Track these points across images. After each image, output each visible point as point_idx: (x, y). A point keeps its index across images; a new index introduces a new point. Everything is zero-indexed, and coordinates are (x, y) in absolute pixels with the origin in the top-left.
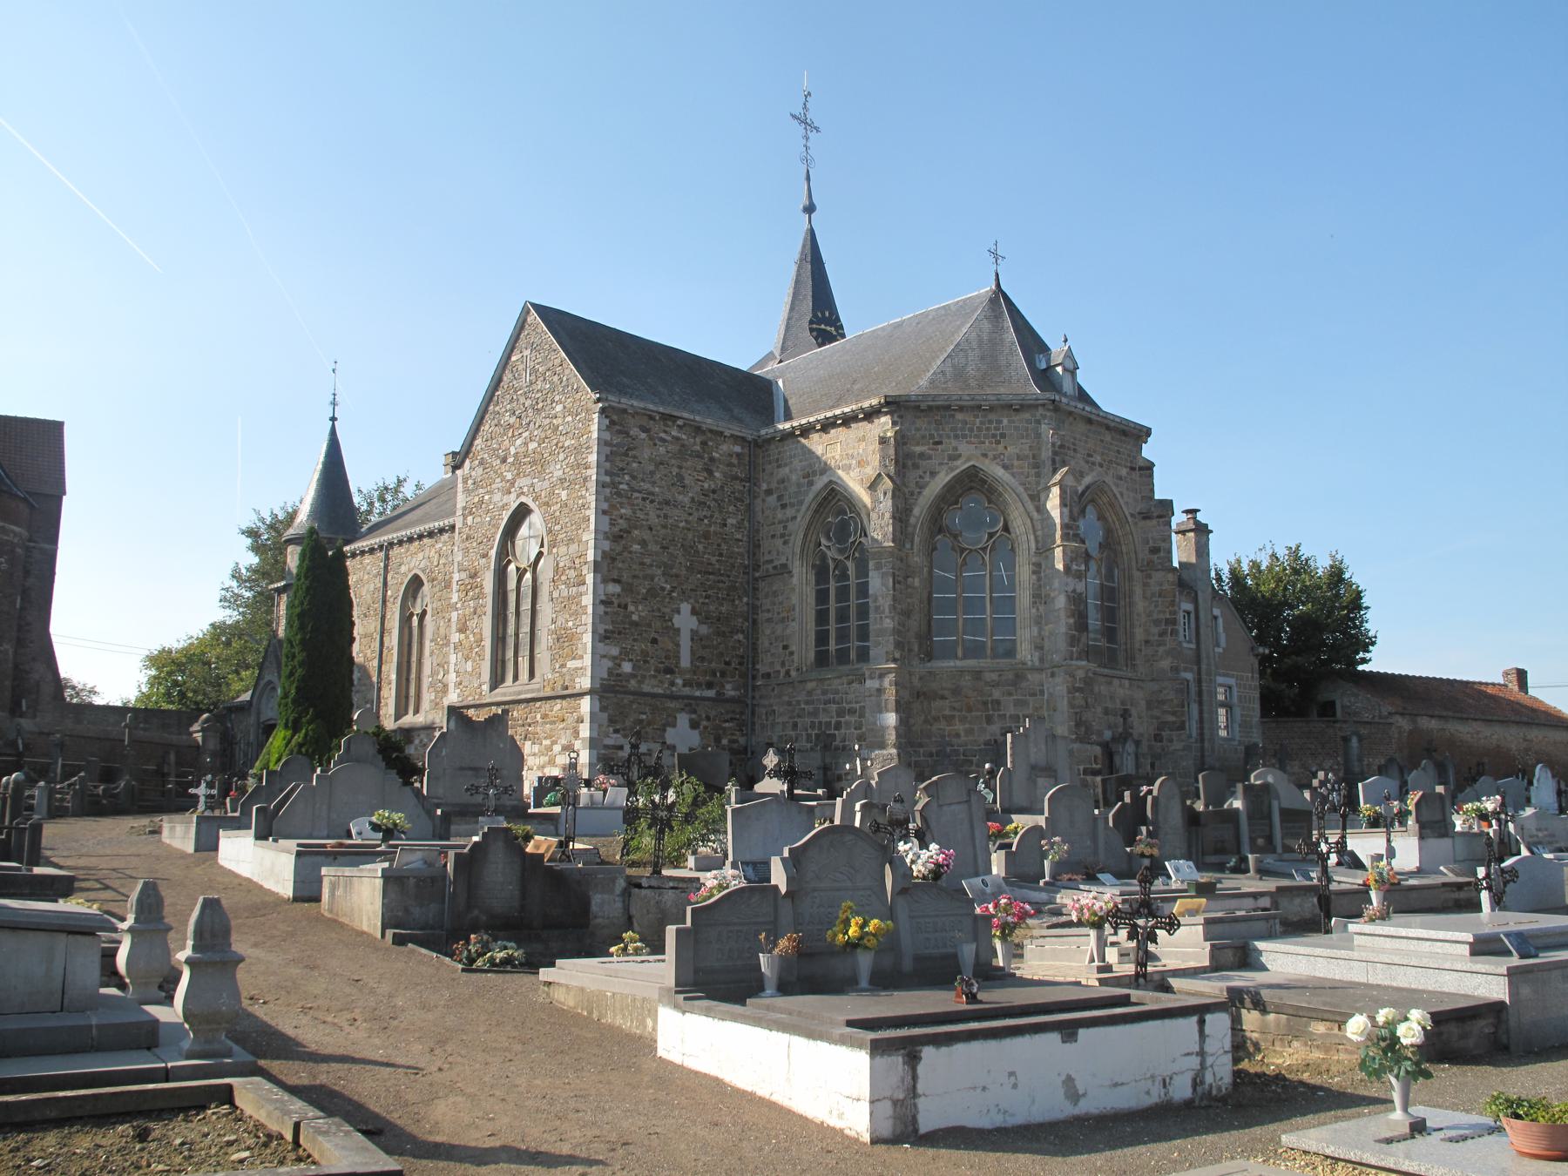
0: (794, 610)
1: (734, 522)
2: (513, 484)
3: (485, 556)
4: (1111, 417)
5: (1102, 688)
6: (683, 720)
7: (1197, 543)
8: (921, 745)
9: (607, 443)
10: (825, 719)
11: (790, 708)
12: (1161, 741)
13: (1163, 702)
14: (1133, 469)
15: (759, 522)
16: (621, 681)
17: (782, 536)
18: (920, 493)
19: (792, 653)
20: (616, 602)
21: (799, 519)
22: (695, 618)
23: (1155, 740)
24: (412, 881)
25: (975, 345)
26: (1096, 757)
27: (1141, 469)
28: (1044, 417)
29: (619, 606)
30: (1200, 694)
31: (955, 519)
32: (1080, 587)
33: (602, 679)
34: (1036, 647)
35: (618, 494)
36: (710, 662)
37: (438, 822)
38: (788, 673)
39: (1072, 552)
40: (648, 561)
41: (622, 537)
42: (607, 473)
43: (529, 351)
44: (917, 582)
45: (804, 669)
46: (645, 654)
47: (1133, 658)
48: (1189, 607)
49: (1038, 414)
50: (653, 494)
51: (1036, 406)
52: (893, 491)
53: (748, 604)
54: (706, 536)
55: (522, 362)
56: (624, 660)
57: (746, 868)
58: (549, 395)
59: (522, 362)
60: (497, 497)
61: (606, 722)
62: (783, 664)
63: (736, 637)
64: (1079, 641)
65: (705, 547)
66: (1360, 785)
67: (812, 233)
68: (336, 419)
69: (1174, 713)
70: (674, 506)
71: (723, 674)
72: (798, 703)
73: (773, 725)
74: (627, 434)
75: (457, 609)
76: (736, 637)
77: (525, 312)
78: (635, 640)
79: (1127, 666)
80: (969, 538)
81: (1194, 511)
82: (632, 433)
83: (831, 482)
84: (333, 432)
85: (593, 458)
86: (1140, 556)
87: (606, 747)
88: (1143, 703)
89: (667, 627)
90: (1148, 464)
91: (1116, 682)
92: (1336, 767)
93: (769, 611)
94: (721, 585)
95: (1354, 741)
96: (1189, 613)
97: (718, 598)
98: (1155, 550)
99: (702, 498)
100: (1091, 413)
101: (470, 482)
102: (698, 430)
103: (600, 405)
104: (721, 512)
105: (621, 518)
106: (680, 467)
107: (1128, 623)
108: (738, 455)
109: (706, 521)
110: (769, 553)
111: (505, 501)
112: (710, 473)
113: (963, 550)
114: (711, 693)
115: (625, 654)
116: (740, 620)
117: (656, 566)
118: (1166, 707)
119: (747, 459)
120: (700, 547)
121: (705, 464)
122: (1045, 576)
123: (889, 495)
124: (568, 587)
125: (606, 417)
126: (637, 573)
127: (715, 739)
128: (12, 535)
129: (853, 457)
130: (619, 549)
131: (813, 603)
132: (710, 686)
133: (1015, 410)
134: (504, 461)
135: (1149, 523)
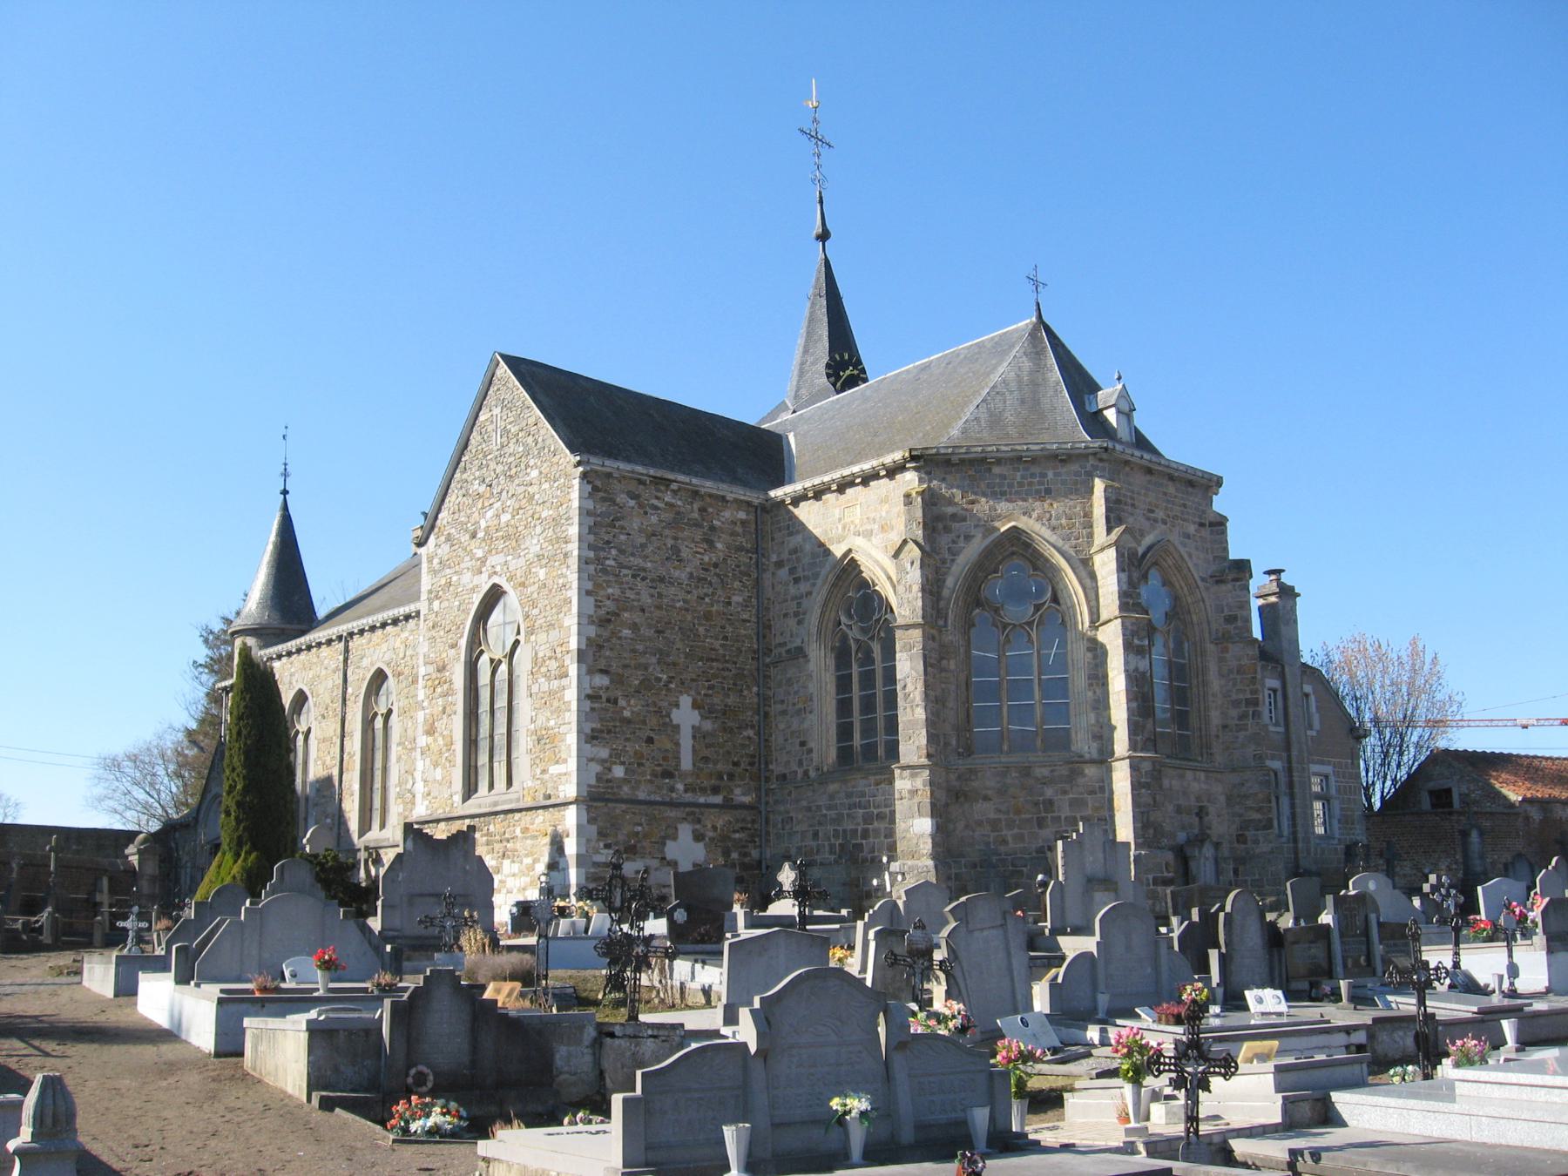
0: (811, 700)
1: (740, 599)
2: (483, 561)
3: (454, 646)
4: (1175, 466)
6: (685, 831)
11: (809, 814)
13: (1246, 797)
14: (1202, 525)
16: (612, 788)
17: (796, 614)
18: (953, 560)
19: (810, 751)
21: (814, 594)
22: (696, 712)
23: (1238, 842)
25: (1013, 386)
26: (1167, 864)
27: (1211, 524)
29: (608, 701)
30: (1291, 785)
31: (996, 589)
33: (589, 786)
35: (605, 571)
36: (715, 763)
39: (1133, 624)
40: (640, 648)
43: (499, 409)
48: (1274, 683)
50: (644, 570)
51: (1085, 456)
56: (615, 763)
58: (523, 459)
60: (467, 577)
62: (800, 763)
64: (1144, 727)
68: (288, 492)
69: (1259, 810)
70: (669, 582)
71: (731, 776)
72: (819, 807)
75: (423, 708)
76: (745, 734)
78: (627, 740)
79: (1202, 756)
80: (1016, 613)
81: (1278, 572)
83: (850, 551)
84: (285, 507)
85: (574, 531)
86: (1214, 626)
87: (596, 864)
88: (1222, 799)
89: (665, 724)
90: (1219, 519)
94: (726, 673)
96: (1275, 691)
98: (1231, 619)
99: (703, 574)
101: (436, 561)
103: (581, 469)
106: (676, 539)
108: (743, 522)
109: (707, 600)
111: (475, 583)
112: (711, 543)
113: (1005, 626)
114: (718, 799)
115: (616, 756)
118: (1249, 803)
119: (754, 526)
120: (701, 630)
121: (705, 534)
123: (917, 564)
125: (588, 482)
130: (606, 634)
132: (715, 790)
133: (1062, 461)
134: (474, 536)
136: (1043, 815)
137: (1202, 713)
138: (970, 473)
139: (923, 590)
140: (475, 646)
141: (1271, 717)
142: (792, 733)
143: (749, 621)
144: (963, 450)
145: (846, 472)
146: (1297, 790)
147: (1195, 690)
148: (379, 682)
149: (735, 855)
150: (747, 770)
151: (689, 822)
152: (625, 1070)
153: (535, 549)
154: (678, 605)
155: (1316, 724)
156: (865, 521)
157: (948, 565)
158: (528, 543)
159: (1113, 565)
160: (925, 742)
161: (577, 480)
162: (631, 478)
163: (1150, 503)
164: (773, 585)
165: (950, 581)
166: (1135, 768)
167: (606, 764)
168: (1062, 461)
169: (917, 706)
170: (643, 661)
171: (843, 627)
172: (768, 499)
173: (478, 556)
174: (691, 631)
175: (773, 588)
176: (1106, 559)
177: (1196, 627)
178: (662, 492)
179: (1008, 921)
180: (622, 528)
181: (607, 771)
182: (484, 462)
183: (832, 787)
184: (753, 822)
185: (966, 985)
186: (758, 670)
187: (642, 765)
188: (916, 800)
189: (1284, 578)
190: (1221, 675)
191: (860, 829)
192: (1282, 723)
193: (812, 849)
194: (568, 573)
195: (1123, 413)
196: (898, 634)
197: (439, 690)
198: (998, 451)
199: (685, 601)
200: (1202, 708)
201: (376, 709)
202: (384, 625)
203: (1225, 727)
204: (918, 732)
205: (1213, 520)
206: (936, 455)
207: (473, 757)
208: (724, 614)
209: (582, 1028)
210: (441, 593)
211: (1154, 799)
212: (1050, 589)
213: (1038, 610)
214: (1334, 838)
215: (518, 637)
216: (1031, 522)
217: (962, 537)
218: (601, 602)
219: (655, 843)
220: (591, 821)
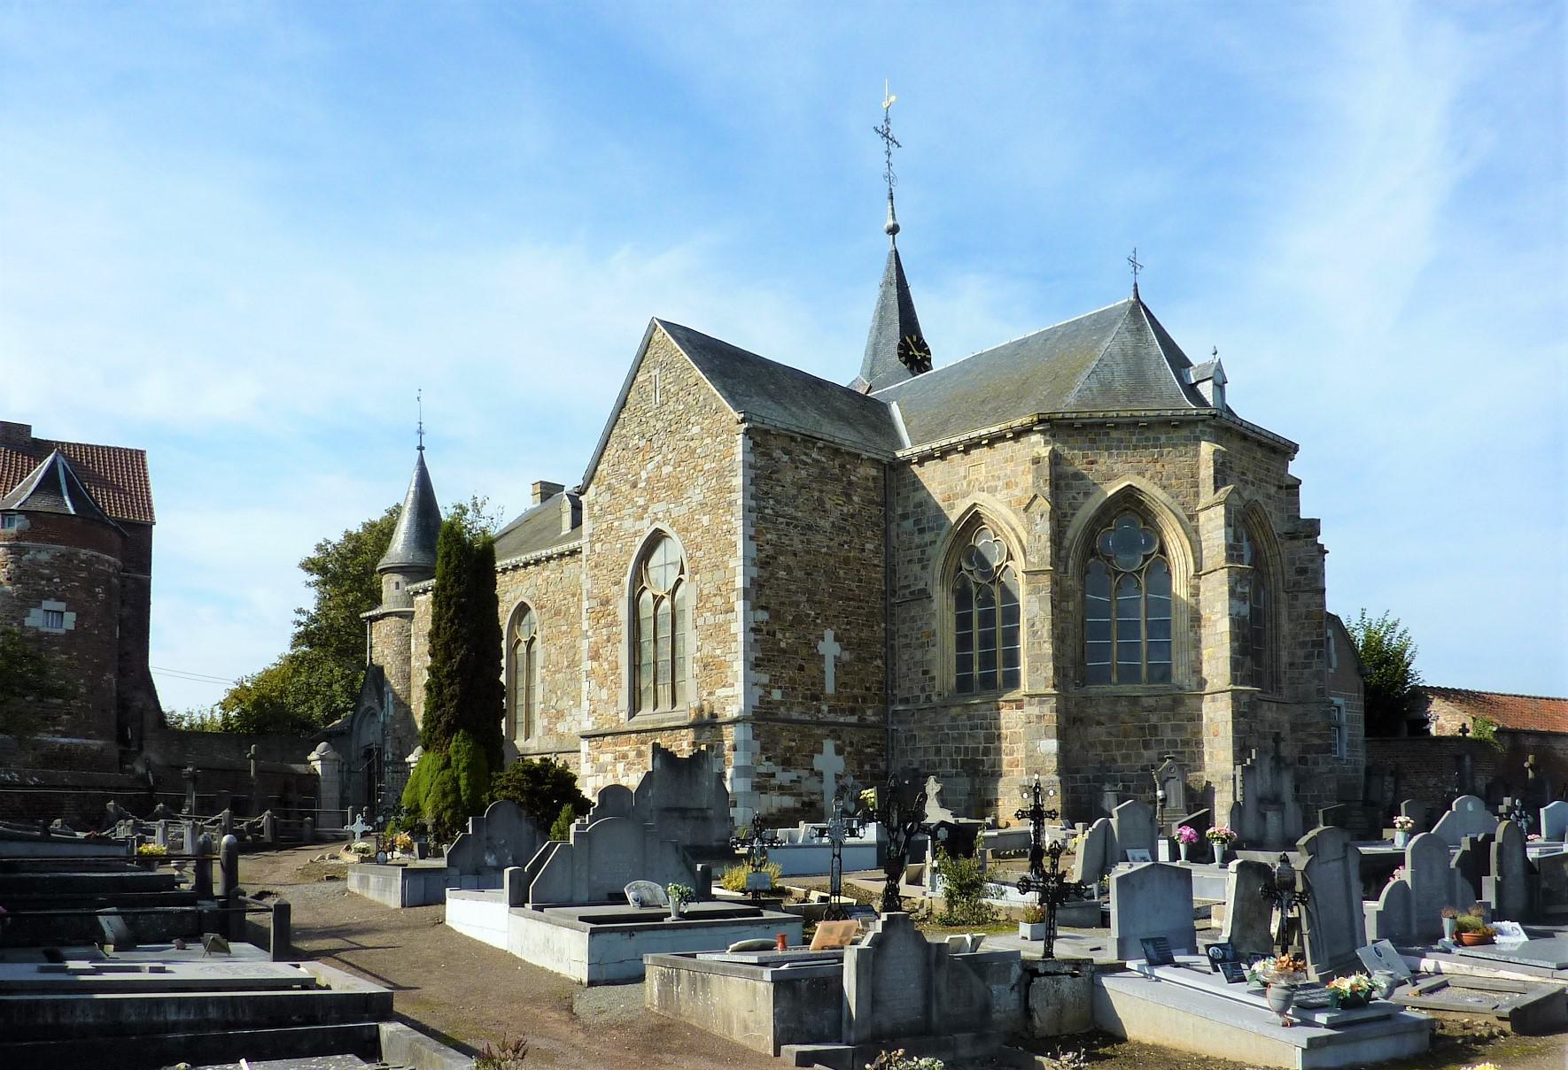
0: (934, 635)
2: (645, 508)
3: (617, 583)
4: (1258, 430)
6: (829, 746)
8: (1077, 771)
10: (970, 744)
11: (932, 733)
13: (1309, 725)
14: (1280, 487)
15: (894, 548)
17: (921, 560)
18: (1073, 514)
19: (933, 678)
20: (765, 629)
21: (939, 543)
22: (837, 644)
24: (804, 984)
25: (1119, 359)
27: (1288, 487)
33: (753, 707)
34: (1194, 672)
35: (764, 518)
36: (852, 688)
37: (699, 878)
38: (928, 698)
39: (1237, 573)
40: (793, 587)
43: (658, 371)
47: (1278, 681)
49: (1198, 431)
50: (795, 518)
54: (846, 561)
55: (651, 383)
57: (1147, 947)
58: (684, 416)
59: (651, 383)
60: (628, 523)
61: (758, 750)
62: (923, 689)
63: (875, 663)
64: (1243, 665)
68: (423, 448)
69: (1320, 736)
71: (864, 700)
72: (941, 728)
73: (913, 750)
75: (588, 637)
76: (875, 663)
77: (652, 328)
78: (783, 667)
79: (1272, 690)
80: (1122, 561)
82: (774, 455)
83: (975, 504)
84: (422, 463)
85: (738, 481)
87: (760, 775)
88: (1287, 726)
89: (813, 654)
92: (1440, 785)
93: (906, 636)
95: (1468, 759)
99: (843, 524)
101: (596, 508)
102: (836, 452)
103: (745, 426)
104: (859, 536)
107: (1274, 645)
108: (874, 478)
109: (846, 546)
110: (906, 577)
111: (637, 528)
112: (849, 496)
113: (1117, 573)
114: (853, 719)
116: (879, 646)
119: (883, 482)
120: (841, 572)
122: (1205, 599)
123: (1047, 516)
124: (714, 615)
125: (750, 438)
126: (783, 599)
127: (858, 764)
128: (107, 565)
129: (999, 478)
130: (766, 575)
131: (954, 628)
132: (852, 711)
134: (634, 486)
137: (1274, 652)
138: (1090, 436)
140: (637, 584)
143: (878, 566)
144: (1087, 415)
145: (974, 434)
148: (522, 613)
149: (867, 767)
151: (833, 739)
152: (1050, 1007)
154: (824, 550)
155: (1334, 664)
156: (990, 478)
158: (690, 493)
159: (1222, 521)
160: (1052, 674)
161: (741, 436)
162: (787, 436)
164: (898, 535)
165: (1070, 534)
167: (767, 689)
169: (1045, 642)
170: (794, 599)
171: (964, 572)
172: (895, 458)
173: (639, 504)
174: (834, 573)
175: (898, 538)
176: (1213, 515)
177: (1272, 577)
179: (1349, 854)
180: (779, 481)
181: (767, 694)
182: (644, 419)
183: (954, 711)
185: (1318, 916)
186: (886, 608)
188: (1043, 724)
190: (1291, 620)
191: (981, 747)
193: (935, 764)
194: (733, 519)
197: (603, 621)
200: (1274, 648)
201: (519, 637)
202: (526, 565)
203: (1291, 665)
204: (1045, 665)
205: (1290, 483)
207: (637, 678)
208: (860, 559)
209: (1008, 967)
210: (602, 536)
212: (1158, 541)
214: (1342, 760)
215: (681, 576)
216: (1144, 481)
218: (762, 546)
219: (806, 756)
220: (756, 737)
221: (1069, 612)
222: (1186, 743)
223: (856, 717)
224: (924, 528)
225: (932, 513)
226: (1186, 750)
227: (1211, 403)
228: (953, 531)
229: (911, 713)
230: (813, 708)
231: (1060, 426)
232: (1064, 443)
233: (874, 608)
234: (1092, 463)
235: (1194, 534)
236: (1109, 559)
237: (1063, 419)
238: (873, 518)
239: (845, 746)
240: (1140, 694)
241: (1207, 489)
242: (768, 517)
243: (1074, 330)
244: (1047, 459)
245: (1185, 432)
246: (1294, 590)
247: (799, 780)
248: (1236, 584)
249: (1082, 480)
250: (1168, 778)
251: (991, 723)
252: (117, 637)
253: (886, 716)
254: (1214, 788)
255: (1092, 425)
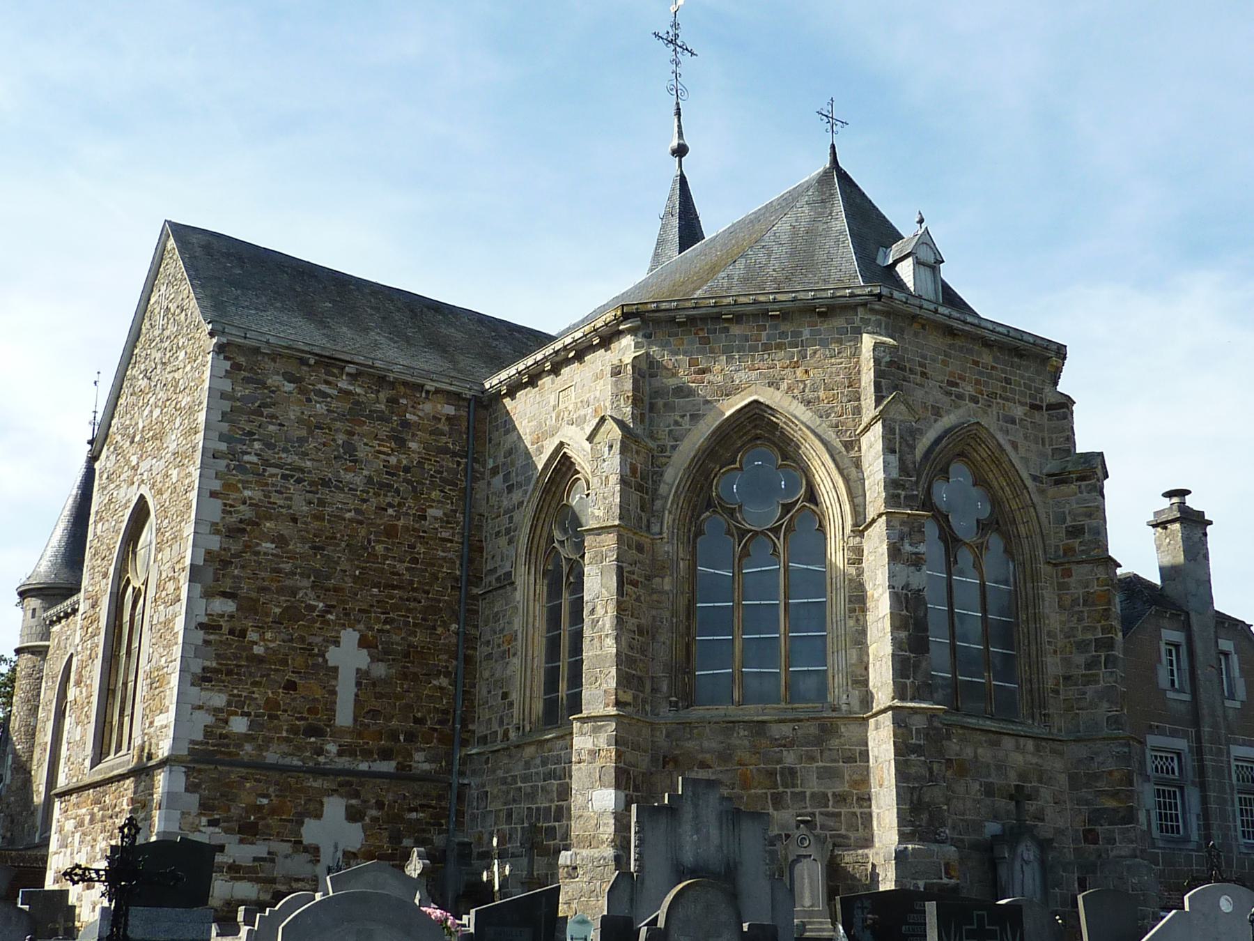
0: (516, 639)
1: (439, 513)
4: (990, 326)
5: (980, 751)
6: (335, 807)
7: (1186, 540)
9: (224, 396)
11: (504, 788)
12: (1095, 842)
13: (1095, 777)
16: (228, 746)
17: (508, 531)
18: (674, 448)
19: (511, 704)
20: (226, 627)
22: (365, 651)
23: (1086, 840)
26: (947, 865)
27: (1050, 407)
28: (866, 322)
29: (231, 632)
30: (1201, 771)
31: (732, 486)
32: (918, 580)
33: (193, 742)
34: (855, 682)
35: (241, 468)
39: (903, 523)
40: (287, 567)
41: (244, 530)
42: (222, 438)
44: (667, 584)
45: (527, 728)
46: (272, 705)
47: (1043, 705)
48: (1177, 636)
49: (857, 319)
50: (302, 470)
51: (854, 308)
52: (622, 442)
53: (457, 634)
54: (391, 532)
56: (236, 714)
61: (195, 809)
62: (501, 722)
65: (386, 549)
66: (258, 915)
67: (683, 180)
69: (1114, 795)
70: (337, 487)
71: (411, 737)
73: (484, 816)
74: (263, 385)
78: (255, 684)
79: (1033, 719)
81: (1184, 493)
82: (269, 382)
83: (562, 444)
86: (1052, 541)
88: (1063, 779)
90: (1064, 400)
91: (1008, 743)
94: (412, 605)
96: (1177, 646)
97: (407, 623)
98: (1075, 532)
99: (386, 478)
100: (949, 317)
102: (382, 381)
103: (215, 340)
104: (416, 498)
105: (244, 503)
106: (351, 433)
108: (449, 419)
109: (390, 511)
112: (401, 444)
113: (743, 533)
114: (388, 766)
115: (237, 705)
116: (445, 657)
117: (302, 575)
118: (1102, 785)
120: (379, 548)
121: (393, 430)
123: (617, 447)
125: (226, 358)
130: (235, 548)
132: (386, 755)
133: (821, 314)
135: (1064, 488)
136: (781, 789)
139: (623, 481)
141: (1173, 681)
142: (496, 681)
146: (1210, 778)
147: (1023, 627)
150: (435, 730)
151: (341, 796)
153: (173, 447)
154: (348, 515)
156: (579, 404)
157: (668, 454)
162: (290, 357)
163: (952, 374)
166: (901, 719)
168: (821, 314)
169: (607, 636)
170: (288, 583)
172: (484, 391)
174: (366, 549)
178: (334, 375)
184: (440, 798)
187: (277, 717)
188: (599, 763)
189: (1190, 502)
192: (1187, 687)
195: (924, 264)
196: (588, 541)
198: (736, 303)
199: (357, 511)
205: (1053, 400)
206: (653, 311)
211: (931, 770)
212: (804, 482)
213: (788, 512)
216: (778, 394)
217: (687, 418)
221: (662, 592)
222: (841, 798)
223: (393, 764)
224: (513, 484)
225: (520, 462)
226: (843, 811)
227: (910, 284)
228: (540, 485)
229: (484, 758)
230: (308, 746)
231: (657, 322)
232: (663, 346)
233: (439, 601)
234: (703, 371)
235: (854, 469)
236: (731, 513)
237: (657, 310)
238: (445, 474)
239: (368, 808)
240: (765, 718)
241: (868, 401)
242: (248, 466)
243: (758, 217)
244: (629, 367)
245: (839, 322)
246: (1064, 562)
247: (271, 857)
248: (902, 539)
249: (687, 396)
250: (799, 856)
251: (565, 768)
252: (666, 795)
253: (450, 763)
254: (878, 874)
255: (704, 319)
